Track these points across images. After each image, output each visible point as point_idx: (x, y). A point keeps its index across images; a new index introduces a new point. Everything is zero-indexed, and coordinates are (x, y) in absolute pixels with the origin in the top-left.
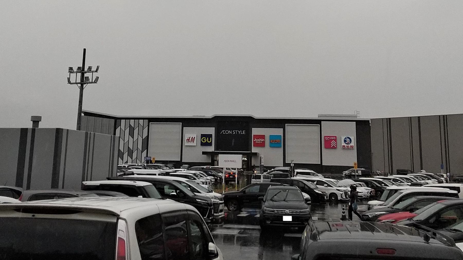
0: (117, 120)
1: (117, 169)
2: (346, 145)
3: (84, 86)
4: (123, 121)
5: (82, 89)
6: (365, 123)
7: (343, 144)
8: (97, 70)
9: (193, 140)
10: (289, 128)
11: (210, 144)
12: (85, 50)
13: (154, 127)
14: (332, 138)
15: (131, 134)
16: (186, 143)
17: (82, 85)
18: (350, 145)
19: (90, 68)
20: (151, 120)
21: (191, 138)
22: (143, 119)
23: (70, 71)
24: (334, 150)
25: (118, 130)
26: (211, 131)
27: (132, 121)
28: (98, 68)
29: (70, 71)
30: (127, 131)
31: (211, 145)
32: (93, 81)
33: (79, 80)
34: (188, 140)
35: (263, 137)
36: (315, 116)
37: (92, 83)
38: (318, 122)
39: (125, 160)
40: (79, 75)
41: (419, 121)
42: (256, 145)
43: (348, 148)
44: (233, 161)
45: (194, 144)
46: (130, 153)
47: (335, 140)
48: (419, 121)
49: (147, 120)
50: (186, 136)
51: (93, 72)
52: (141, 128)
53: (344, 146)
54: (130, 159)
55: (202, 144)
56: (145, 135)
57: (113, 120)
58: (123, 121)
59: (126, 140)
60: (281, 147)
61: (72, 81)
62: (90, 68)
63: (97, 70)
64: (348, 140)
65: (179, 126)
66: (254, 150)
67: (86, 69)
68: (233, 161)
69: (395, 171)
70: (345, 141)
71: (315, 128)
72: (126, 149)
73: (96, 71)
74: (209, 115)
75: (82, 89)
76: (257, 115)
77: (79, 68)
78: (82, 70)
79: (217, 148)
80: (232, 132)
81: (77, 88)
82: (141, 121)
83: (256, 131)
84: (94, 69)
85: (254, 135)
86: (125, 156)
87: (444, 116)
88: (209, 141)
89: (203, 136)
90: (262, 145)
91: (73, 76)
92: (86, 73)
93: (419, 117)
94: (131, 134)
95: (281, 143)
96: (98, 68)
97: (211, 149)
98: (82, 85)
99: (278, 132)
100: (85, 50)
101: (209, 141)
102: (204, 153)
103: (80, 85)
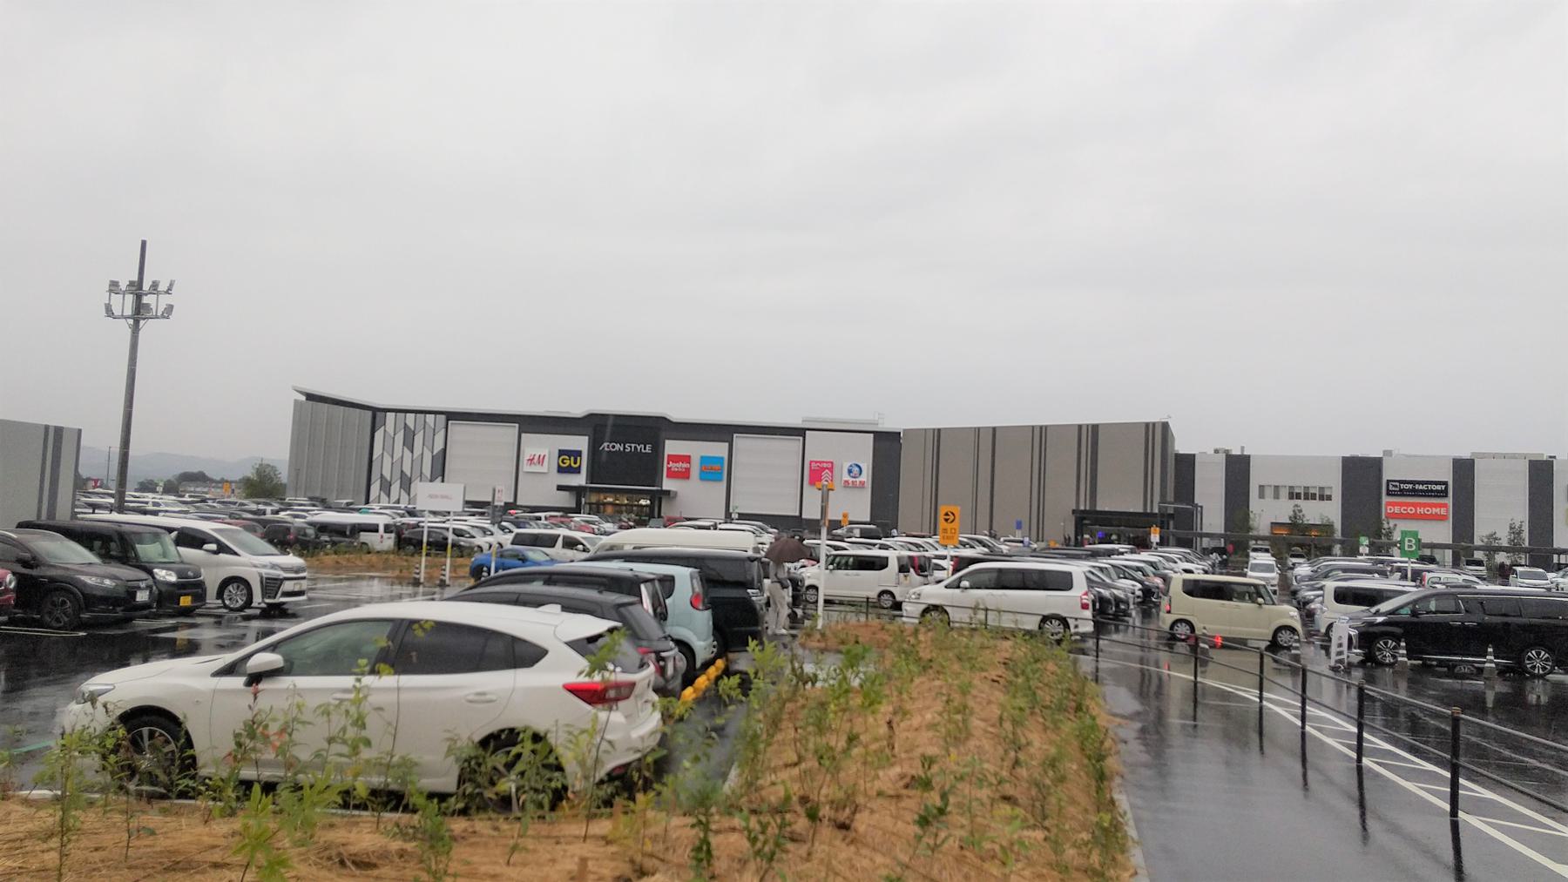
0: (377, 414)
1: (74, 491)
2: (851, 480)
3: (142, 322)
4: (391, 416)
5: (136, 329)
6: (895, 436)
7: (846, 477)
8: (170, 289)
9: (541, 460)
10: (740, 441)
11: (578, 471)
12: (144, 244)
13: (458, 430)
14: (825, 465)
15: (409, 443)
16: (525, 467)
17: (137, 322)
18: (858, 480)
19: (155, 285)
20: (452, 416)
21: (536, 458)
22: (436, 413)
23: (113, 288)
24: (856, 491)
25: (379, 435)
26: (581, 443)
27: (410, 417)
28: (171, 285)
29: (113, 288)
30: (400, 437)
31: (579, 472)
32: (159, 314)
33: (128, 311)
34: (531, 460)
35: (687, 459)
36: (796, 422)
37: (157, 317)
38: (800, 432)
39: (394, 496)
40: (130, 298)
41: (994, 435)
42: (673, 475)
43: (854, 486)
44: (446, 497)
45: (544, 469)
46: (406, 484)
47: (831, 470)
48: (994, 435)
49: (443, 417)
50: (527, 453)
51: (158, 293)
52: (429, 433)
53: (847, 482)
54: (404, 495)
55: (561, 470)
56: (439, 446)
57: (369, 414)
58: (391, 416)
59: (397, 455)
60: (721, 480)
61: (117, 311)
62: (155, 285)
63: (170, 289)
64: (856, 470)
65: (514, 429)
66: (668, 484)
67: (146, 287)
68: (446, 497)
69: (735, 516)
70: (850, 471)
71: (794, 444)
72: (397, 474)
73: (168, 292)
74: (578, 410)
75: (136, 329)
76: (677, 415)
77: (131, 284)
78: (136, 288)
79: (592, 477)
80: (625, 448)
81: (124, 327)
82: (430, 418)
83: (672, 447)
84: (163, 287)
85: (669, 456)
86: (395, 487)
87: (1041, 427)
88: (575, 463)
89: (562, 453)
90: (685, 475)
91: (116, 300)
92: (146, 295)
93: (994, 429)
94: (409, 443)
95: (721, 473)
96: (171, 285)
97: (580, 480)
98: (137, 322)
99: (718, 449)
100: (144, 244)
101: (575, 463)
102: (560, 488)
103: (131, 321)
